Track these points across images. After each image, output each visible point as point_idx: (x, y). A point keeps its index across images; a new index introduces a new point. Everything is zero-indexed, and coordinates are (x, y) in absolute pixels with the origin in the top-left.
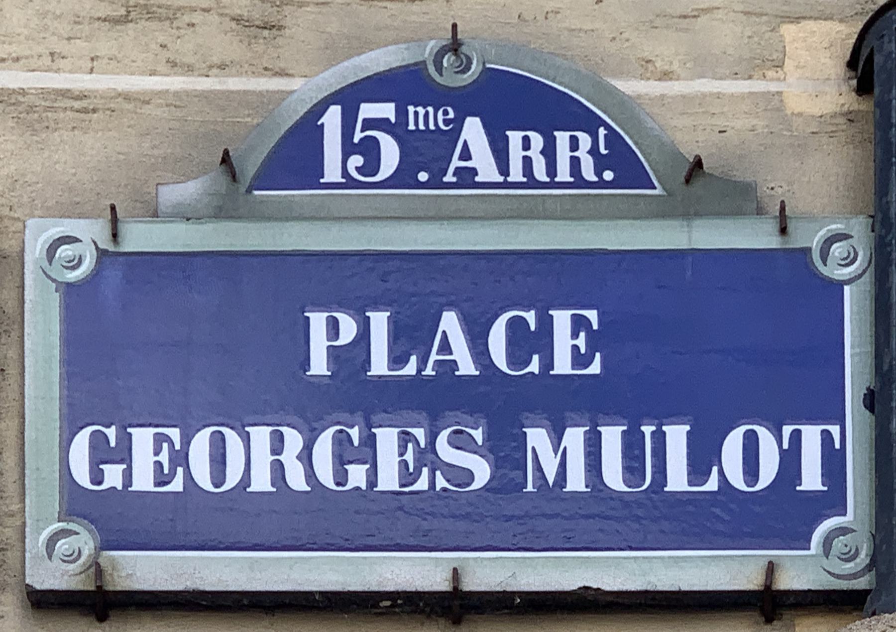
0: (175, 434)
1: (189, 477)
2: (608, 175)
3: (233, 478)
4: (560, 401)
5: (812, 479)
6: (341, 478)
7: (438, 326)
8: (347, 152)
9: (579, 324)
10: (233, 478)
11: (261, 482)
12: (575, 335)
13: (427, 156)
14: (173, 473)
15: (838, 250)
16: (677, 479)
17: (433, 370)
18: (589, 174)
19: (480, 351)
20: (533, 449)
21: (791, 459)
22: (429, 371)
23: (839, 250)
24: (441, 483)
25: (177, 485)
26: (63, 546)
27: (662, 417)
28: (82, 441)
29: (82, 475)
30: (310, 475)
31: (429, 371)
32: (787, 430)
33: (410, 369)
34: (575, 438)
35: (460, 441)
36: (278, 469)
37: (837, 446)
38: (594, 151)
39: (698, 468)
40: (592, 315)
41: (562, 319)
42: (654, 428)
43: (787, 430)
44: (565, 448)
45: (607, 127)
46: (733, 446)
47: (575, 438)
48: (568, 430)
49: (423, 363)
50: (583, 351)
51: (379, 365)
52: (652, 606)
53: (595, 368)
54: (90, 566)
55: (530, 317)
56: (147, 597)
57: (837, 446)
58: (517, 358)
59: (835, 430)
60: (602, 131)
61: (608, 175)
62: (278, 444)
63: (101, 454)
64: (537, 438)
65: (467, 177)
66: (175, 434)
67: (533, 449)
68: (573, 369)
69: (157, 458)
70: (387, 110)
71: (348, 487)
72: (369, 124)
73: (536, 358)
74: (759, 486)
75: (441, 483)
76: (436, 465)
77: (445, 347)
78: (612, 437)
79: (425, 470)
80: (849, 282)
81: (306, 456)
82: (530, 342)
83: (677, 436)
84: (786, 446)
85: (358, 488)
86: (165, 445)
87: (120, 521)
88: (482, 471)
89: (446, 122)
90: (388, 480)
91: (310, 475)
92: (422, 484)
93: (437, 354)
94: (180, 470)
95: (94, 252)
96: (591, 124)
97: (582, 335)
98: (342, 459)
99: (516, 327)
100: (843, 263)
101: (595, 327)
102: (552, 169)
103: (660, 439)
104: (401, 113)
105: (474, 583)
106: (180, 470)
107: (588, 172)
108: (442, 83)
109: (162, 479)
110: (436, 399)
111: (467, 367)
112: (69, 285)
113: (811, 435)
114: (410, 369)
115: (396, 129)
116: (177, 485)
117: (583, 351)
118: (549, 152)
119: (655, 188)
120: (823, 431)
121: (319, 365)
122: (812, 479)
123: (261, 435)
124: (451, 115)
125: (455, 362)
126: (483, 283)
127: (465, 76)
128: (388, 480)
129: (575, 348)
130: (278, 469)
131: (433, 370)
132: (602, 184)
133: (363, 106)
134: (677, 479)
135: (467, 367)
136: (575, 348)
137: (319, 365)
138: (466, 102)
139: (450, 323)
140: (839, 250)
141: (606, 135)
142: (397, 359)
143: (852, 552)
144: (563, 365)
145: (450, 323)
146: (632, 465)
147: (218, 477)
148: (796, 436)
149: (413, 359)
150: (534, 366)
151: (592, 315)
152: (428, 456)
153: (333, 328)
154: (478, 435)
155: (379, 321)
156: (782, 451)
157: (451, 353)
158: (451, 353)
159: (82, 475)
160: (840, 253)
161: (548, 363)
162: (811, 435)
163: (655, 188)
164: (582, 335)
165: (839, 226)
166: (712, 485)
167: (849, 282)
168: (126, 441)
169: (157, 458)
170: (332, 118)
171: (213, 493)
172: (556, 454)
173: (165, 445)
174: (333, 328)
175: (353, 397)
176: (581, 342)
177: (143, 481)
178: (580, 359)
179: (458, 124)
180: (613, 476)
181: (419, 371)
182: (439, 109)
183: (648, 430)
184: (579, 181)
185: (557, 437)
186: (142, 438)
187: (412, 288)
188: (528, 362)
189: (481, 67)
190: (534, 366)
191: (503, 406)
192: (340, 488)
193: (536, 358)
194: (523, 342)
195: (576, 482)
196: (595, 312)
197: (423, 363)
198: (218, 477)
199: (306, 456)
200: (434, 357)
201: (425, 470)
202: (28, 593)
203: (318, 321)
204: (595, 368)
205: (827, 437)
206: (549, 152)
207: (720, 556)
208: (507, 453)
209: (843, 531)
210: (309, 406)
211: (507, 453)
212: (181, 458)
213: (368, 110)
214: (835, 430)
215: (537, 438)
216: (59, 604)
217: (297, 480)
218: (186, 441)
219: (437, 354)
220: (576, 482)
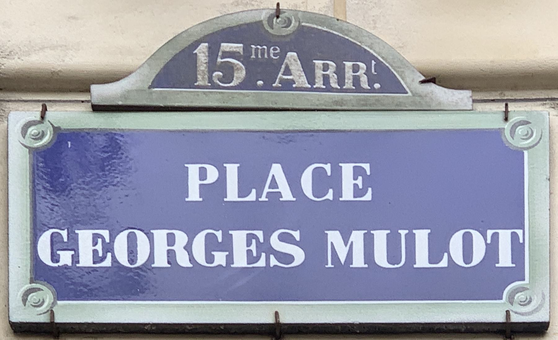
0: (105, 233)
2: (377, 86)
3: (141, 260)
4: (348, 218)
5: (505, 259)
6: (210, 258)
7: (269, 172)
8: (211, 71)
9: (358, 172)
10: (141, 260)
11: (161, 261)
12: (355, 178)
13: (263, 73)
14: (258, 258)
15: (520, 130)
16: (422, 260)
17: (266, 197)
18: (365, 85)
20: (332, 243)
21: (492, 249)
22: (263, 198)
23: (520, 130)
25: (107, 263)
26: (33, 297)
27: (412, 227)
28: (45, 239)
30: (192, 259)
31: (263, 198)
32: (490, 233)
33: (252, 197)
34: (357, 237)
35: (285, 238)
36: (171, 254)
37: (521, 241)
40: (366, 167)
41: (347, 169)
42: (407, 231)
43: (490, 233)
44: (352, 242)
45: (376, 59)
47: (357, 237)
48: (354, 232)
49: (259, 195)
50: (361, 187)
51: (232, 195)
52: (173, 333)
53: (368, 197)
54: (48, 311)
55: (328, 167)
56: (391, 326)
57: (521, 241)
58: (318, 190)
59: (519, 232)
60: (373, 63)
61: (377, 86)
64: (334, 237)
65: (288, 85)
66: (105, 233)
67: (332, 243)
68: (239, 197)
69: (249, 248)
70: (238, 47)
71: (60, 264)
72: (227, 54)
73: (331, 191)
74: (474, 263)
75: (273, 262)
76: (271, 251)
77: (274, 184)
78: (380, 237)
79: (263, 255)
80: (527, 149)
81: (188, 248)
82: (327, 182)
83: (422, 236)
84: (489, 241)
85: (220, 266)
86: (254, 241)
87: (68, 283)
88: (299, 256)
89: (275, 55)
91: (192, 259)
92: (261, 263)
93: (269, 188)
94: (109, 255)
95: (52, 129)
96: (366, 57)
97: (360, 178)
98: (211, 245)
99: (318, 174)
100: (525, 137)
101: (368, 173)
103: (411, 239)
104: (247, 49)
105: (285, 319)
106: (109, 255)
108: (274, 33)
109: (97, 259)
110: (263, 216)
111: (287, 195)
112: (37, 149)
113: (505, 236)
114: (252, 197)
115: (245, 58)
116: (107, 263)
117: (361, 187)
118: (340, 73)
119: (407, 93)
120: (512, 233)
121: (194, 195)
122: (505, 259)
123: (160, 235)
124: (279, 51)
125: (280, 192)
126: (294, 149)
127: (289, 28)
128: (240, 261)
129: (356, 185)
130: (171, 254)
131: (266, 197)
133: (222, 44)
134: (422, 260)
135: (287, 195)
136: (356, 185)
137: (194, 195)
138: (286, 45)
140: (520, 130)
141: (375, 65)
142: (243, 191)
143: (528, 300)
144: (348, 195)
145: (276, 170)
147: (132, 260)
148: (495, 237)
149: (254, 191)
150: (330, 196)
151: (366, 167)
152: (266, 248)
153: (203, 174)
154: (296, 235)
155: (232, 170)
156: (487, 244)
157: (278, 188)
158: (278, 188)
160: (521, 132)
161: (338, 193)
163: (407, 93)
164: (360, 178)
165: (523, 117)
166: (444, 263)
167: (527, 149)
168: (228, 239)
169: (249, 248)
171: (463, 267)
172: (346, 247)
173: (254, 241)
174: (203, 174)
175: (215, 213)
176: (359, 181)
177: (86, 260)
178: (358, 192)
179: (283, 56)
180: (381, 259)
181: (257, 198)
182: (270, 47)
184: (358, 88)
186: (85, 236)
187: (254, 154)
189: (297, 24)
190: (330, 196)
191: (314, 219)
192: (56, 265)
193: (331, 191)
195: (359, 262)
196: (368, 165)
197: (259, 195)
198: (132, 260)
199: (188, 248)
200: (267, 190)
201: (263, 255)
202: (11, 326)
203: (193, 170)
204: (368, 197)
205: (514, 237)
206: (340, 73)
207: (226, 304)
208: (315, 246)
210: (190, 220)
211: (315, 246)
212: (109, 248)
213: (226, 46)
214: (519, 232)
215: (334, 237)
216: (21, 332)
217: (183, 260)
218: (112, 238)
219: (269, 188)
220: (359, 262)
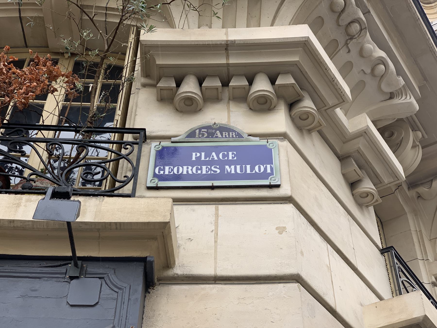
0: (172, 167)
1: (173, 172)
4: (230, 163)
5: (269, 171)
9: (233, 154)
19: (218, 156)
21: (266, 169)
24: (212, 172)
25: (172, 173)
27: (246, 164)
29: (157, 172)
32: (265, 166)
33: (208, 159)
34: (233, 167)
38: (235, 134)
39: (251, 170)
40: (235, 153)
43: (265, 166)
46: (257, 168)
47: (233, 167)
49: (209, 159)
51: (203, 158)
62: (188, 168)
63: (160, 169)
66: (172, 167)
70: (206, 130)
75: (212, 172)
76: (211, 170)
81: (192, 170)
83: (248, 167)
90: (204, 172)
91: (192, 172)
92: (209, 173)
98: (197, 169)
102: (229, 136)
105: (214, 185)
107: (234, 136)
110: (211, 163)
111: (216, 158)
114: (208, 159)
115: (207, 132)
121: (194, 159)
122: (269, 171)
132: (236, 138)
134: (248, 171)
137: (194, 159)
139: (214, 154)
142: (205, 157)
144: (230, 158)
146: (241, 170)
148: (266, 166)
150: (226, 158)
151: (235, 153)
153: (196, 155)
155: (203, 154)
159: (157, 172)
162: (268, 166)
166: (254, 172)
170: (197, 131)
175: (199, 162)
176: (233, 155)
178: (233, 158)
179: (216, 132)
180: (238, 171)
183: (244, 166)
185: (230, 167)
188: (124, 45)
190: (226, 158)
191: (222, 164)
194: (224, 156)
197: (209, 159)
203: (194, 154)
204: (235, 158)
205: (271, 166)
208: (222, 169)
209: (273, 177)
212: (172, 170)
215: (227, 167)
217: (190, 172)
218: (174, 168)
220: (233, 172)
